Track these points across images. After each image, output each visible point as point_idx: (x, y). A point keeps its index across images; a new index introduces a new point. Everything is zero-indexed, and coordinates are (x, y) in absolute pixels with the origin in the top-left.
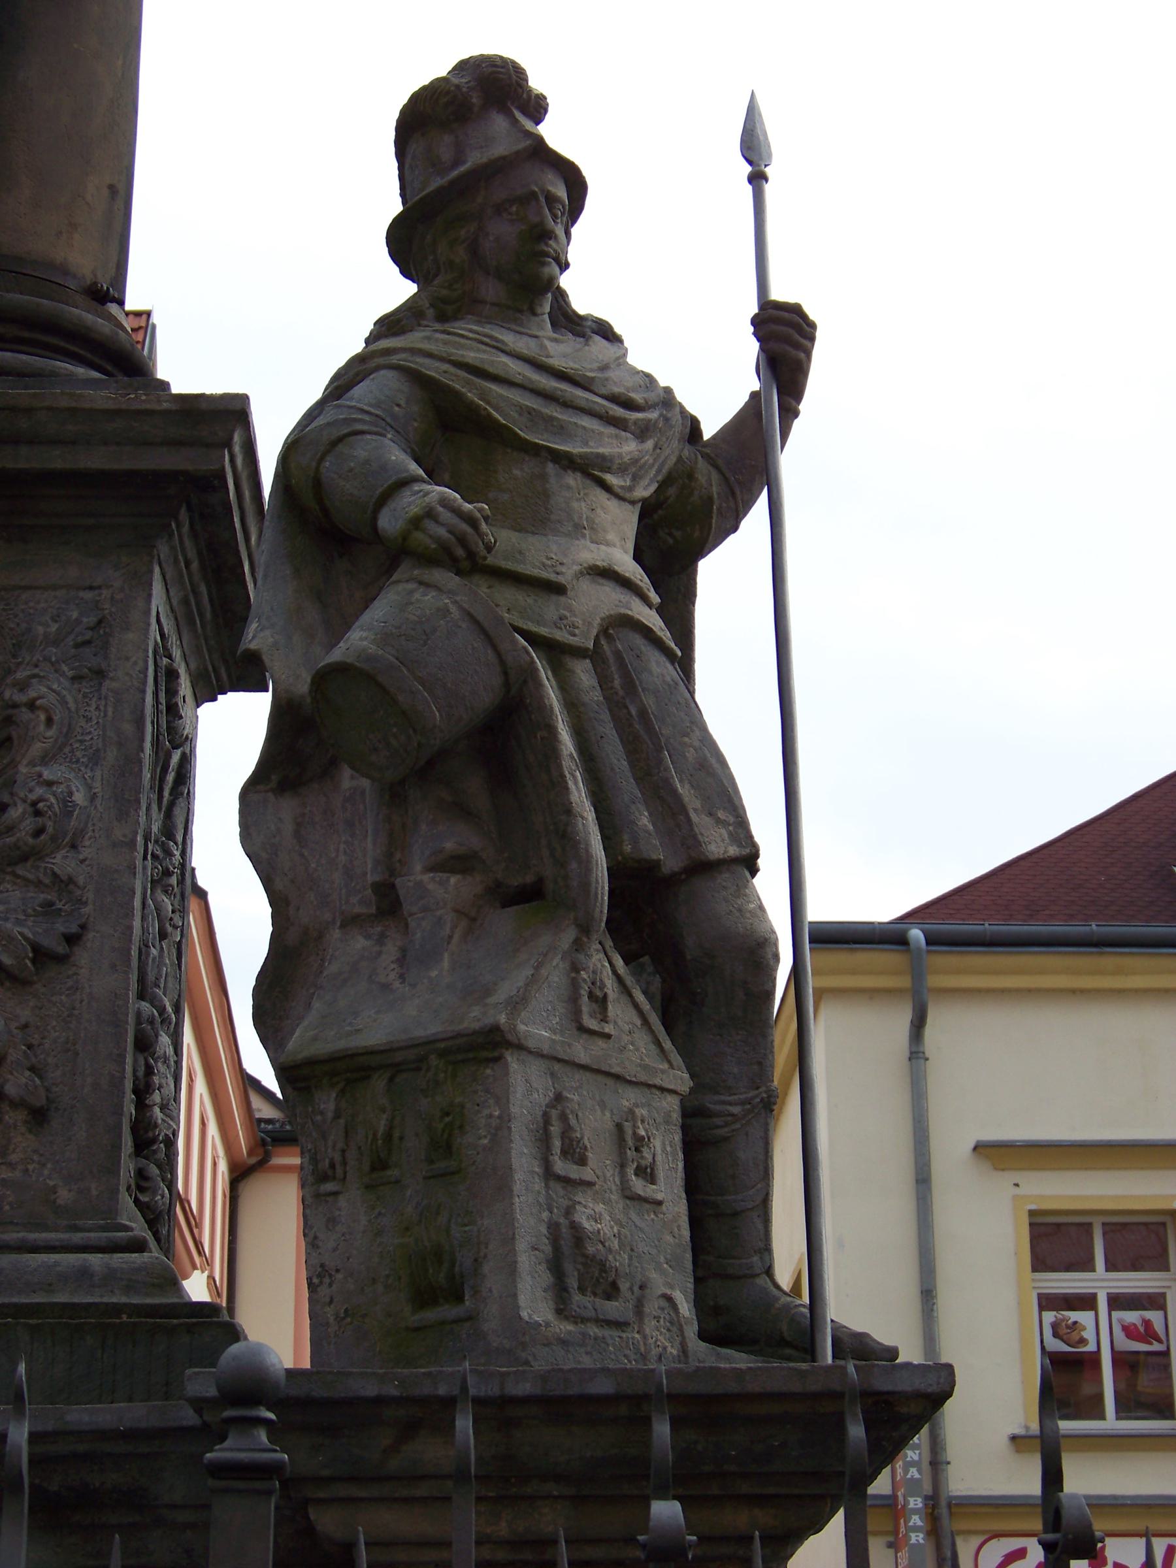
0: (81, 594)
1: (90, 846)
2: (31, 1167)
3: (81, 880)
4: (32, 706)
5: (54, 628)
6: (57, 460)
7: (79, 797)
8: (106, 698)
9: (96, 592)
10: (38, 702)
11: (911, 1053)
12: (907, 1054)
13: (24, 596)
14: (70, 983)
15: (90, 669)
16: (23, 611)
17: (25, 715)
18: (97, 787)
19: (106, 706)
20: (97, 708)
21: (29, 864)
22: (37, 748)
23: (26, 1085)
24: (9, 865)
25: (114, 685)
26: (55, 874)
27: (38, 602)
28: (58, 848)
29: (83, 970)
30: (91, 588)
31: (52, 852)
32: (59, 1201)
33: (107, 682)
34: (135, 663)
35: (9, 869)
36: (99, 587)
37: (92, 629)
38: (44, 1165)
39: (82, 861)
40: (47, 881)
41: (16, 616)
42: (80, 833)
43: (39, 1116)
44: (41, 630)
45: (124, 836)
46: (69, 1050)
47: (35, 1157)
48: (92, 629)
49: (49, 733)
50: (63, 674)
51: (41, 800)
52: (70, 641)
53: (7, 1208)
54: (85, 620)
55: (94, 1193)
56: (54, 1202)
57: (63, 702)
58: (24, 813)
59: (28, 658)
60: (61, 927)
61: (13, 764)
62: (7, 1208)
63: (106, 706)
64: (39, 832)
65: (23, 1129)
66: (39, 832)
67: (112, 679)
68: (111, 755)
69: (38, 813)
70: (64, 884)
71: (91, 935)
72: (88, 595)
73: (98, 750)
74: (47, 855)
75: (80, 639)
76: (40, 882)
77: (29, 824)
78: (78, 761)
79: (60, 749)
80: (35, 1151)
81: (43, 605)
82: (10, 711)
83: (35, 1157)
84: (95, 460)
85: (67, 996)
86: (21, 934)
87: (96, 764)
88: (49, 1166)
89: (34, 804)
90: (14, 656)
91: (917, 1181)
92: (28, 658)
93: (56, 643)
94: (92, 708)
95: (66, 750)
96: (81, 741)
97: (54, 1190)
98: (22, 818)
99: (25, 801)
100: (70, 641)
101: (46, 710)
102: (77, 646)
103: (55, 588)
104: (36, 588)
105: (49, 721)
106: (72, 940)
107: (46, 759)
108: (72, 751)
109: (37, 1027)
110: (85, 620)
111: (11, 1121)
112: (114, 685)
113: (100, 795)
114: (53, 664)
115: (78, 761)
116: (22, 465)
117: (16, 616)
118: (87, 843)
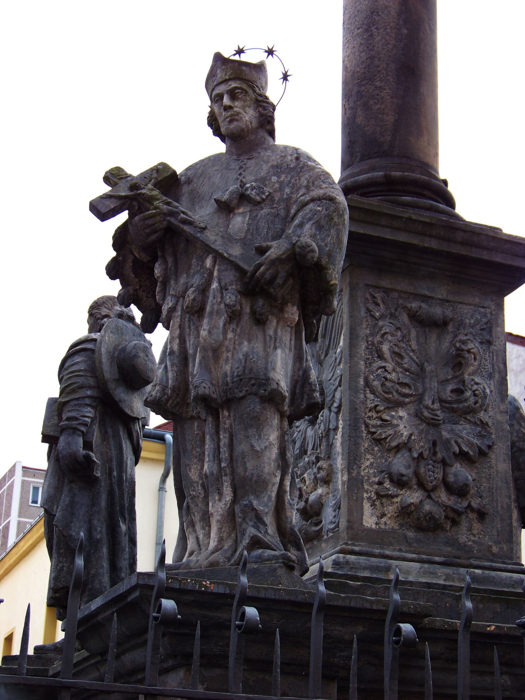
0: (480, 309)
1: (491, 411)
2: (481, 537)
3: (490, 424)
4: (469, 351)
5: (472, 321)
6: (485, 256)
7: (488, 391)
8: (493, 353)
9: (485, 309)
10: (472, 350)
11: (160, 488)
12: (158, 488)
13: (459, 306)
14: (489, 465)
15: (486, 340)
16: (459, 312)
17: (467, 355)
18: (492, 388)
19: (493, 356)
20: (489, 356)
21: (471, 415)
22: (471, 369)
23: (479, 504)
24: (463, 414)
25: (495, 348)
26: (481, 421)
27: (464, 309)
28: (481, 410)
29: (493, 461)
30: (483, 307)
31: (479, 412)
32: (494, 552)
33: (493, 347)
34: (502, 340)
35: (464, 416)
36: (486, 308)
37: (485, 324)
38: (485, 536)
39: (490, 417)
40: (479, 423)
41: (457, 314)
42: (488, 406)
43: (482, 515)
44: (467, 321)
45: (504, 409)
46: (490, 492)
47: (482, 533)
48: (485, 324)
49: (475, 364)
50: (477, 340)
51: (477, 390)
52: (478, 327)
53: (475, 552)
54: (483, 320)
55: (505, 549)
56: (492, 551)
57: (479, 352)
58: (471, 394)
59: (463, 332)
60: (487, 442)
61: (463, 374)
62: (475, 552)
63: (493, 356)
64: (476, 403)
65: (476, 521)
66: (476, 403)
67: (495, 346)
68: (497, 376)
69: (475, 395)
70: (484, 425)
71: (495, 447)
72: (482, 310)
73: (491, 373)
74: (477, 412)
75: (482, 327)
76: (476, 423)
77: (472, 399)
78: (484, 376)
79: (478, 370)
80: (482, 530)
81: (466, 311)
82: (459, 352)
83: (482, 533)
84: (498, 258)
85: (488, 470)
86: (476, 443)
87: (491, 378)
88: (487, 537)
89: (474, 391)
90: (458, 330)
91: (157, 544)
92: (463, 332)
93: (473, 327)
94: (487, 356)
95: (479, 371)
96: (485, 369)
97: (491, 547)
98: (470, 397)
99: (471, 390)
100: (478, 327)
101: (474, 354)
102: (481, 330)
103: (470, 305)
104: (464, 304)
105: (475, 359)
106: (490, 447)
107: (474, 373)
108: (481, 372)
109: (478, 481)
110: (483, 320)
111: (472, 517)
112: (495, 348)
113: (494, 391)
114: (474, 336)
115: (484, 376)
116: (474, 255)
117: (457, 314)
118: (490, 410)
